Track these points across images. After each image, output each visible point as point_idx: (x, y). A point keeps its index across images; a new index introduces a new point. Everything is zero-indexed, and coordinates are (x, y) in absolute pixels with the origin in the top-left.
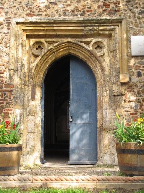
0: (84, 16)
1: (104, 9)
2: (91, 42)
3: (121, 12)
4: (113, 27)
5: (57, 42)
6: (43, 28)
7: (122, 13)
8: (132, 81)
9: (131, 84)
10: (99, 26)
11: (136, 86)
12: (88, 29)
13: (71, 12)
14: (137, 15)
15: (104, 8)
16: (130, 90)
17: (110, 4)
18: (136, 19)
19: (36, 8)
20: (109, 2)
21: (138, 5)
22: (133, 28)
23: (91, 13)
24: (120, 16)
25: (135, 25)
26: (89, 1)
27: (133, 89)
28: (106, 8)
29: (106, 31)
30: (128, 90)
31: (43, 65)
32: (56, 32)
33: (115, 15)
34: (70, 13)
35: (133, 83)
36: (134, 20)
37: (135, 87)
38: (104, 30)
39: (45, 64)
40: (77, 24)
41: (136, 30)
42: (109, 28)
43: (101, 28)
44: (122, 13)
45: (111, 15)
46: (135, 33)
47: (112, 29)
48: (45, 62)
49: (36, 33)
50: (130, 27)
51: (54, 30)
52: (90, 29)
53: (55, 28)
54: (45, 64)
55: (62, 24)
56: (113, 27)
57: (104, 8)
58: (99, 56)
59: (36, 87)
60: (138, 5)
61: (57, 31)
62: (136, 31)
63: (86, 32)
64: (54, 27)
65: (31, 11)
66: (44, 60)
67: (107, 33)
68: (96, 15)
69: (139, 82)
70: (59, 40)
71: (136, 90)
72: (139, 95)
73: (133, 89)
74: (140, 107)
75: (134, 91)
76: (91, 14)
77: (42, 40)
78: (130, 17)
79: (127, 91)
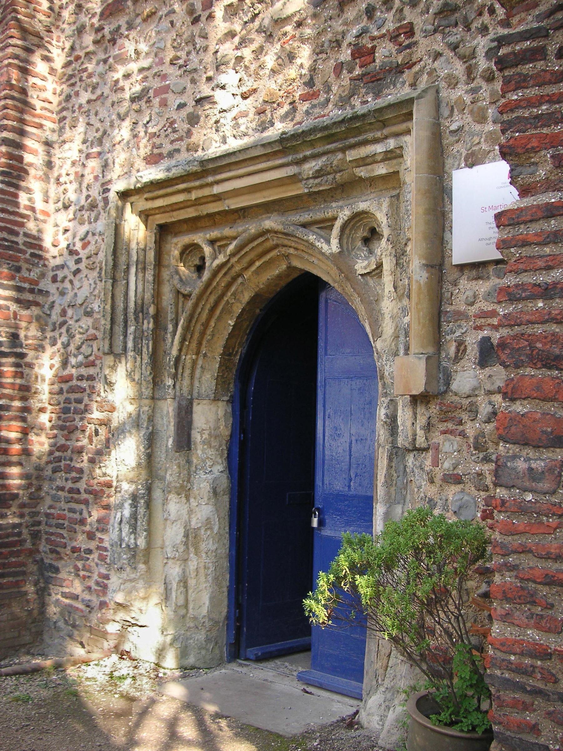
0: (292, 120)
1: (358, 71)
2: (335, 219)
3: (416, 68)
4: (392, 143)
5: (235, 238)
6: (180, 198)
7: (421, 71)
8: (454, 386)
9: (451, 398)
10: (343, 150)
11: (473, 411)
12: (311, 168)
13: (257, 117)
14: (483, 64)
15: (358, 68)
16: (450, 426)
17: (374, 48)
18: (479, 81)
19: (165, 131)
20: (373, 39)
21: (486, 18)
22: (466, 128)
23: (315, 102)
24: (413, 85)
25: (471, 112)
26: (505, 0)
27: (460, 423)
28: (361, 67)
29: (375, 166)
30: (443, 427)
31: (212, 324)
32: (227, 201)
33: (395, 86)
34: (254, 120)
35: (456, 394)
36: (466, 92)
37: (465, 417)
38: (369, 160)
39: (219, 319)
40: (183, 182)
41: (480, 135)
42: (379, 148)
43: (351, 155)
44: (421, 71)
45: (380, 91)
46: (473, 154)
47: (391, 151)
48: (218, 312)
49: (190, 213)
50: (454, 127)
51: (218, 198)
52: (317, 168)
53: (217, 190)
54: (219, 319)
55: (172, 186)
56: (392, 143)
57: (358, 68)
58: (362, 275)
59: (195, 404)
60: (486, 18)
61: (228, 198)
62: (479, 143)
63: (311, 181)
64: (211, 185)
65: (429, 74)
66: (208, 306)
67: (381, 170)
68: (330, 106)
69: (483, 392)
70: (239, 228)
71: (471, 429)
72: (481, 455)
73: (460, 423)
74: (484, 511)
75: (463, 434)
76: (314, 106)
77: (198, 238)
78: (452, 83)
79: (444, 432)
